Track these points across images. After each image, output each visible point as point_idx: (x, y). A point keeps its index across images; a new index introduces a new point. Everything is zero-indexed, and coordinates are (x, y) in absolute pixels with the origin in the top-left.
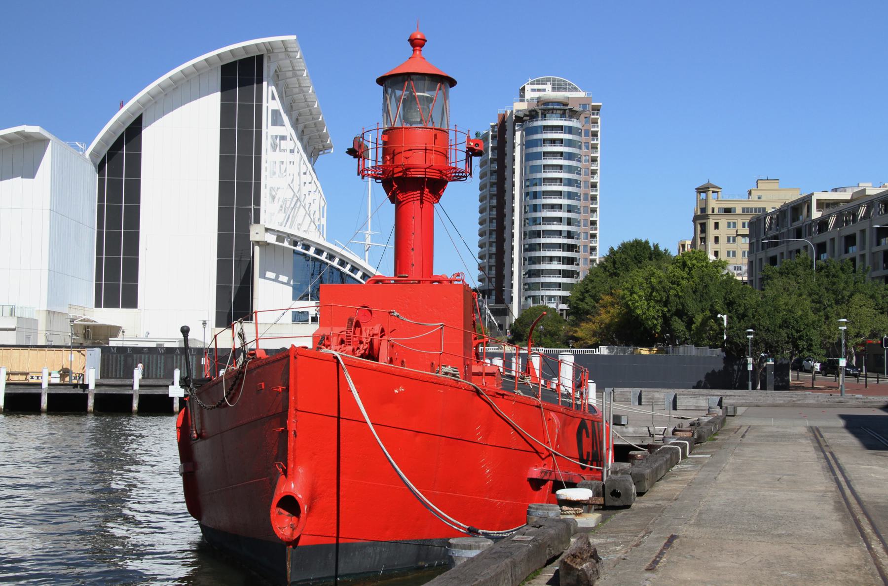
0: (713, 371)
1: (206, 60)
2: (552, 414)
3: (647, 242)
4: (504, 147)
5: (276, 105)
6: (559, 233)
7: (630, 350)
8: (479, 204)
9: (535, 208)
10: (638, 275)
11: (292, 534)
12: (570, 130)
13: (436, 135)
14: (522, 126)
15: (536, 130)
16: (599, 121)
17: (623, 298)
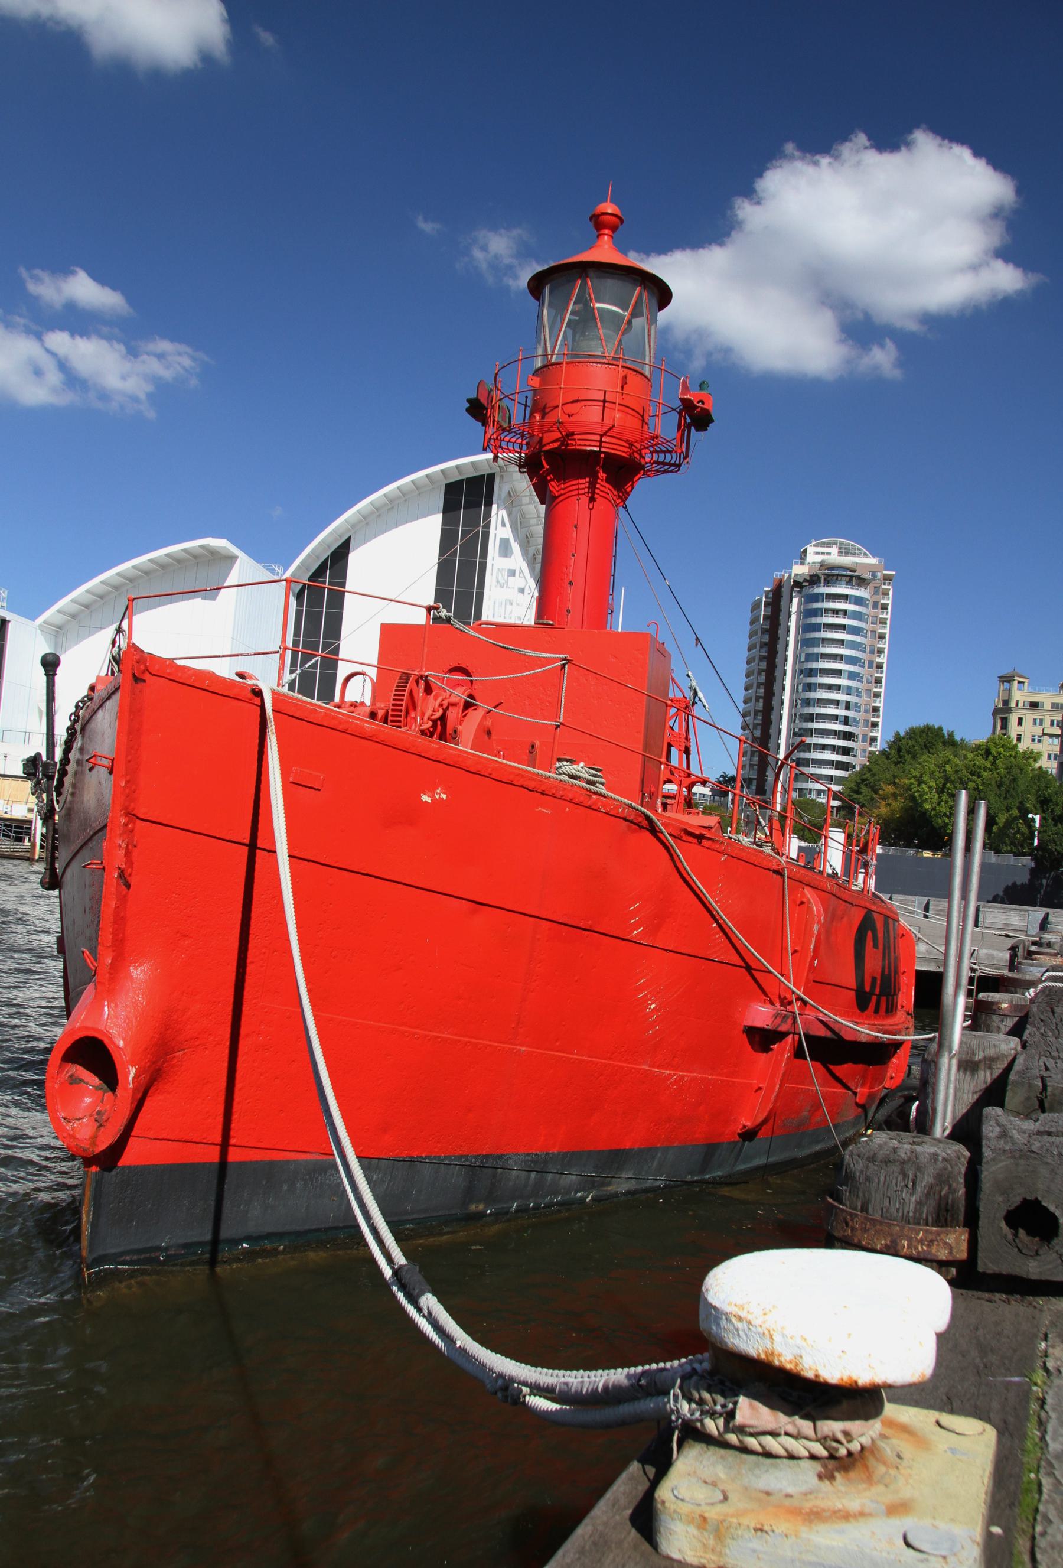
0: (1014, 884)
1: (427, 476)
2: (808, 893)
3: (940, 729)
4: (779, 615)
5: (506, 532)
6: (835, 718)
7: (911, 852)
8: (745, 680)
9: (810, 687)
10: (929, 762)
11: (94, 1138)
12: (858, 601)
13: (625, 377)
14: (800, 592)
15: (817, 598)
16: (891, 593)
17: (909, 789)
